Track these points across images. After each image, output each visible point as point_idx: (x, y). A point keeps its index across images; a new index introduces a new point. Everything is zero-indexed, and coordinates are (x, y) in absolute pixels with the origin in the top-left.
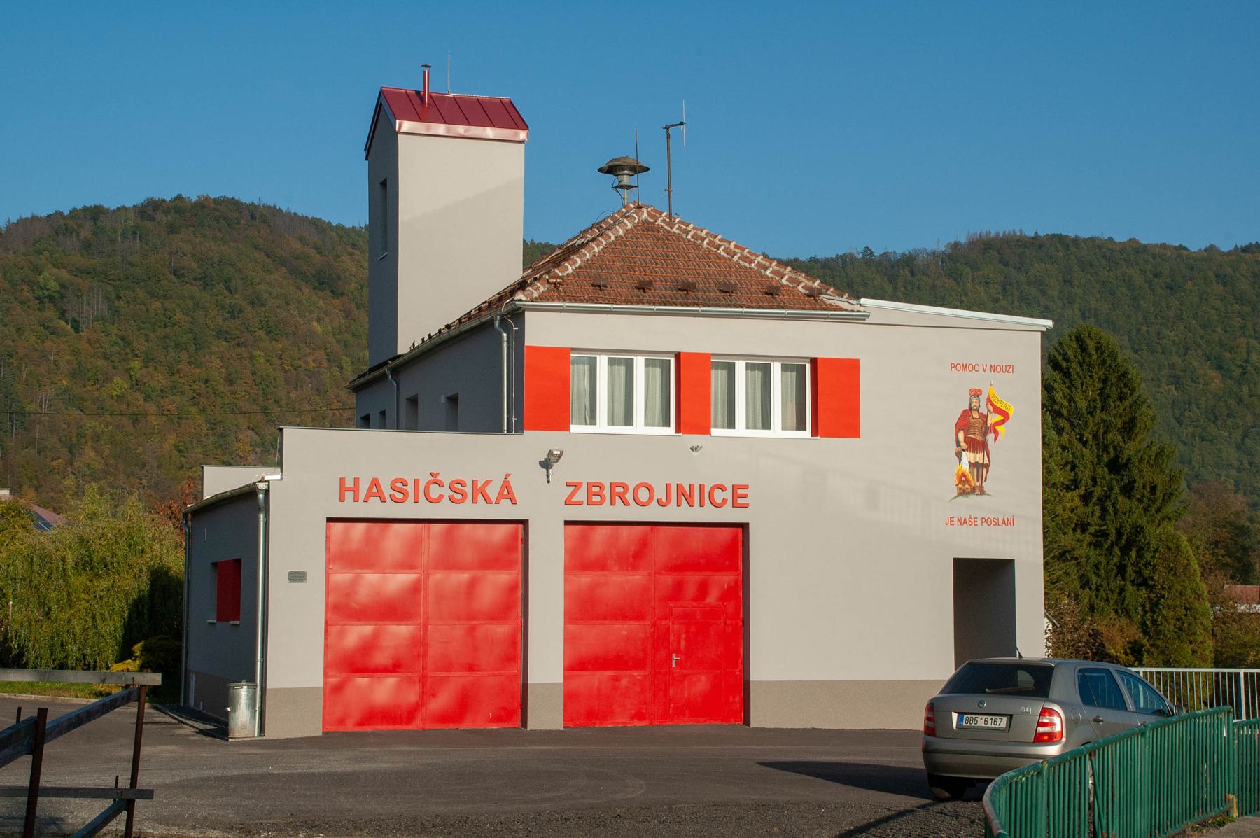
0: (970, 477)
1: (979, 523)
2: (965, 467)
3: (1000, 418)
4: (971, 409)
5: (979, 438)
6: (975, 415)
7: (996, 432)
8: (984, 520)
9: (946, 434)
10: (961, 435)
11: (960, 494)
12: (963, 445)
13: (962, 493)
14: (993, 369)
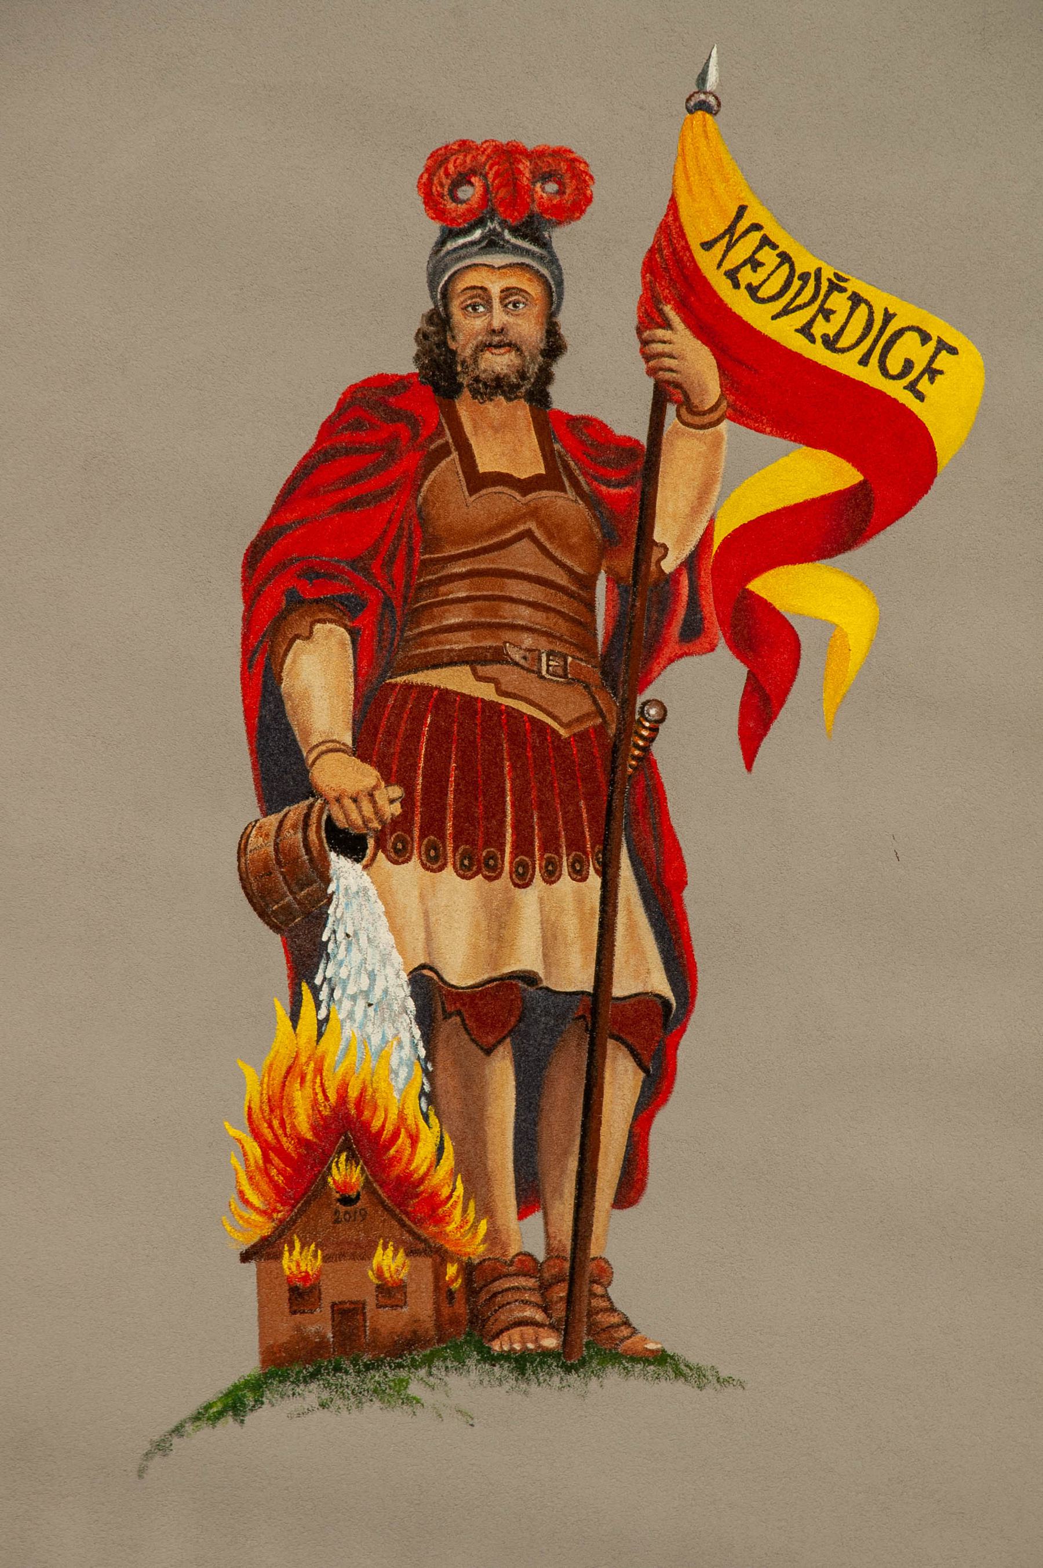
0: (428, 1154)
2: (370, 1037)
3: (810, 473)
4: (441, 370)
5: (559, 707)
6: (503, 443)
7: (771, 653)
10: (321, 675)
11: (289, 1362)
12: (345, 778)
13: (325, 1345)
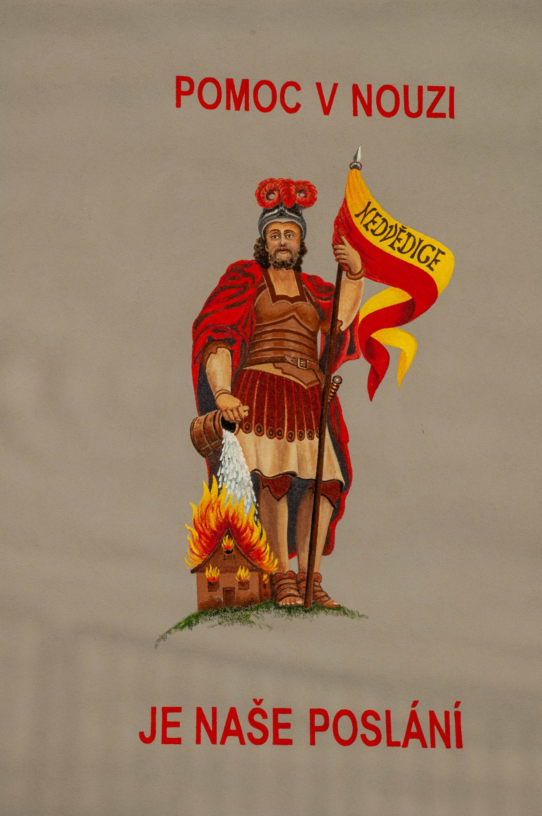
0: (257, 536)
1: (299, 730)
2: (237, 494)
3: (393, 296)
4: (263, 259)
5: (305, 378)
6: (285, 285)
7: (379, 361)
8: (320, 722)
9: (158, 372)
10: (220, 367)
11: (208, 609)
12: (228, 403)
13: (220, 603)
14: (364, 101)
